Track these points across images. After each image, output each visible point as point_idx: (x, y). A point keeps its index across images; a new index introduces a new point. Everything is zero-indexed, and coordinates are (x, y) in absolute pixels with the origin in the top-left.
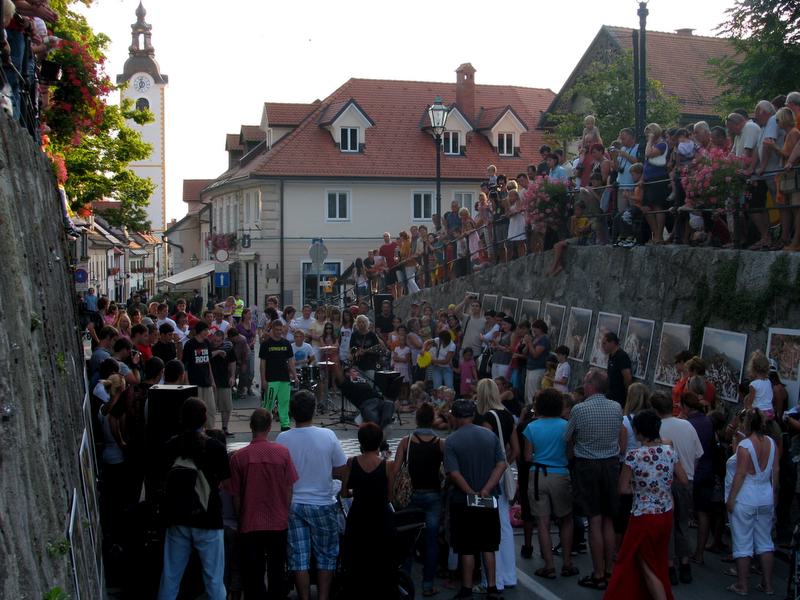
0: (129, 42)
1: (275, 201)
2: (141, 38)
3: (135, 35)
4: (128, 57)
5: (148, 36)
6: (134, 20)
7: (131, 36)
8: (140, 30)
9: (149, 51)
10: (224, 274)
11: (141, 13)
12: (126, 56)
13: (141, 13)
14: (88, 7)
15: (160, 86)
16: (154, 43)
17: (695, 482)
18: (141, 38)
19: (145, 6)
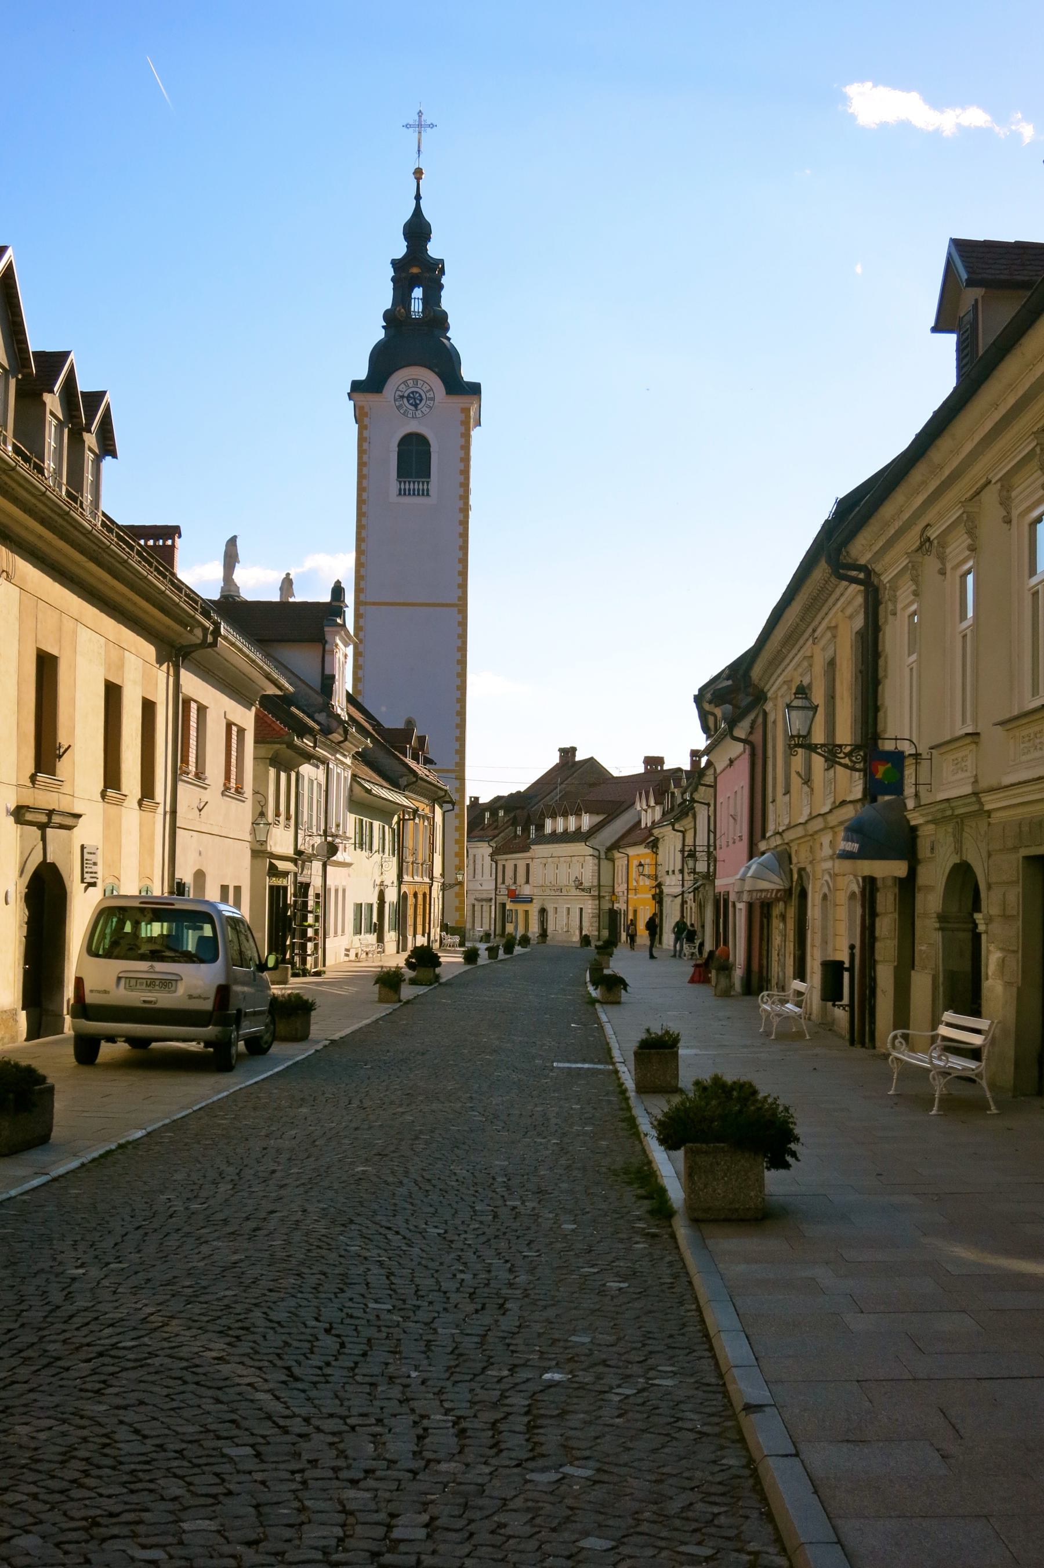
0: (385, 299)
3: (401, 296)
4: (381, 334)
6: (400, 249)
9: (436, 321)
11: (417, 231)
13: (417, 231)
15: (458, 401)
16: (448, 302)
19: (428, 214)
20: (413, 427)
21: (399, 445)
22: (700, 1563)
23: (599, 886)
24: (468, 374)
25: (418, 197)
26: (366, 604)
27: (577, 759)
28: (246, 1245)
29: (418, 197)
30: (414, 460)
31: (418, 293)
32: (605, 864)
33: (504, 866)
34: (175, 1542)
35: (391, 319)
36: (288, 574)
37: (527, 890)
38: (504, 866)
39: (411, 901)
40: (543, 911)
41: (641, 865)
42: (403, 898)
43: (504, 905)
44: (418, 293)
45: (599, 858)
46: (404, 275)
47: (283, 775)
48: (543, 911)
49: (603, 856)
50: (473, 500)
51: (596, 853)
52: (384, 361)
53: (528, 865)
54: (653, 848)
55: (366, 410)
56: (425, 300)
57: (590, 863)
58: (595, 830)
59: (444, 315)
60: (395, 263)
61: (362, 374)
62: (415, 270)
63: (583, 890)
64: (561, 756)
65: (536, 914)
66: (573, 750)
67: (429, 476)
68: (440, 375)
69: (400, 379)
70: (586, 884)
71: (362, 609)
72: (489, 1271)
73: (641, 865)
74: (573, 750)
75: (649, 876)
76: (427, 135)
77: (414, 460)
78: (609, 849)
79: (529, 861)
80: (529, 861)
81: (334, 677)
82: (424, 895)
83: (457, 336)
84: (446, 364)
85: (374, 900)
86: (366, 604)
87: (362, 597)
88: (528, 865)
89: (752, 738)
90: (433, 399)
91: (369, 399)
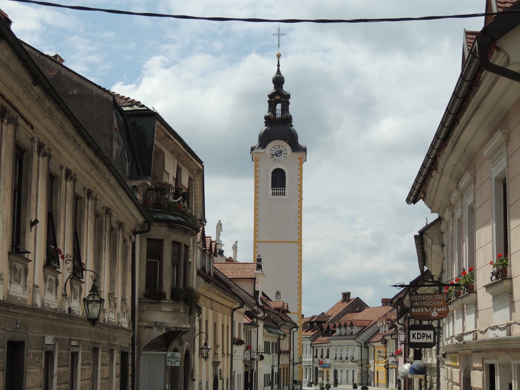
9: (287, 120)
21: (272, 173)
23: (361, 360)
24: (301, 142)
25: (279, 65)
26: (259, 242)
29: (279, 65)
30: (279, 179)
31: (279, 106)
32: (364, 350)
33: (317, 350)
35: (268, 120)
36: (220, 221)
37: (328, 361)
38: (317, 350)
39: (282, 370)
40: (336, 372)
41: (379, 352)
42: (279, 370)
43: (317, 368)
44: (279, 106)
45: (361, 347)
46: (273, 99)
47: (182, 286)
48: (336, 372)
49: (363, 346)
50: (304, 196)
51: (360, 345)
52: (264, 140)
53: (328, 350)
54: (384, 344)
55: (258, 159)
56: (282, 110)
57: (358, 349)
58: (358, 334)
60: (270, 96)
62: (277, 97)
63: (354, 362)
64: (343, 297)
65: (333, 372)
66: (349, 294)
67: (285, 187)
68: (289, 143)
69: (272, 146)
70: (355, 359)
71: (257, 244)
73: (379, 352)
74: (349, 294)
75: (383, 357)
76: (283, 38)
77: (279, 179)
78: (365, 343)
79: (329, 348)
80: (329, 348)
82: (287, 369)
83: (296, 125)
84: (292, 140)
85: (270, 372)
86: (259, 242)
87: (257, 239)
88: (328, 350)
89: (405, 324)
90: (286, 154)
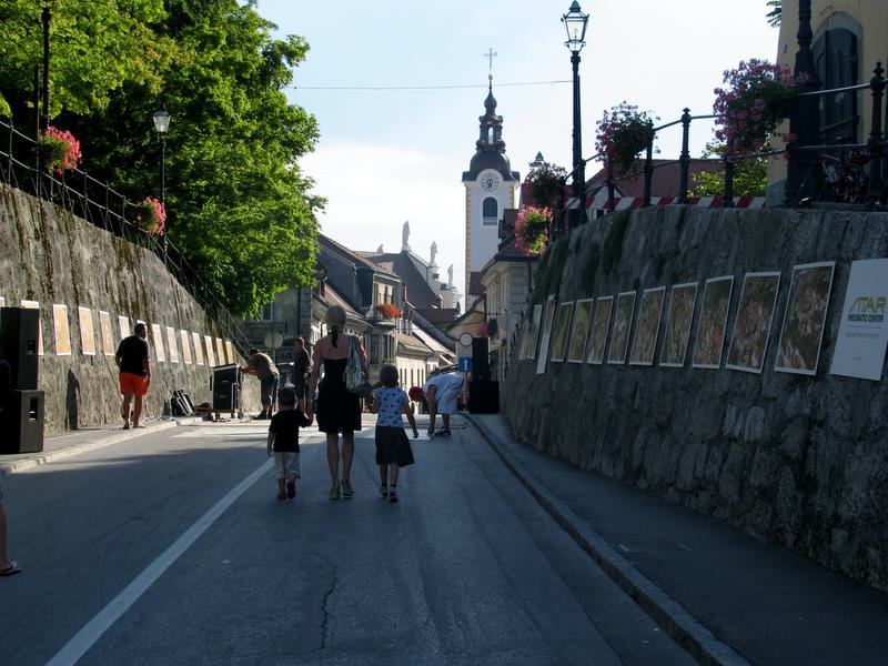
0: (477, 136)
1: (523, 285)
2: (491, 131)
3: (484, 129)
4: (475, 152)
5: (498, 129)
6: (483, 112)
7: (572, 138)
8: (489, 123)
9: (500, 146)
10: (468, 359)
11: (490, 103)
12: (473, 151)
13: (490, 103)
14: (716, 91)
15: (509, 183)
16: (504, 137)
17: (310, 325)
18: (491, 131)
19: (495, 96)
20: (489, 195)
22: (617, 552)
27: (586, 180)
28: (93, 415)
34: (818, 252)
35: (479, 145)
59: (503, 144)
61: (468, 169)
72: (99, 557)
81: (497, 383)
91: (471, 183)
